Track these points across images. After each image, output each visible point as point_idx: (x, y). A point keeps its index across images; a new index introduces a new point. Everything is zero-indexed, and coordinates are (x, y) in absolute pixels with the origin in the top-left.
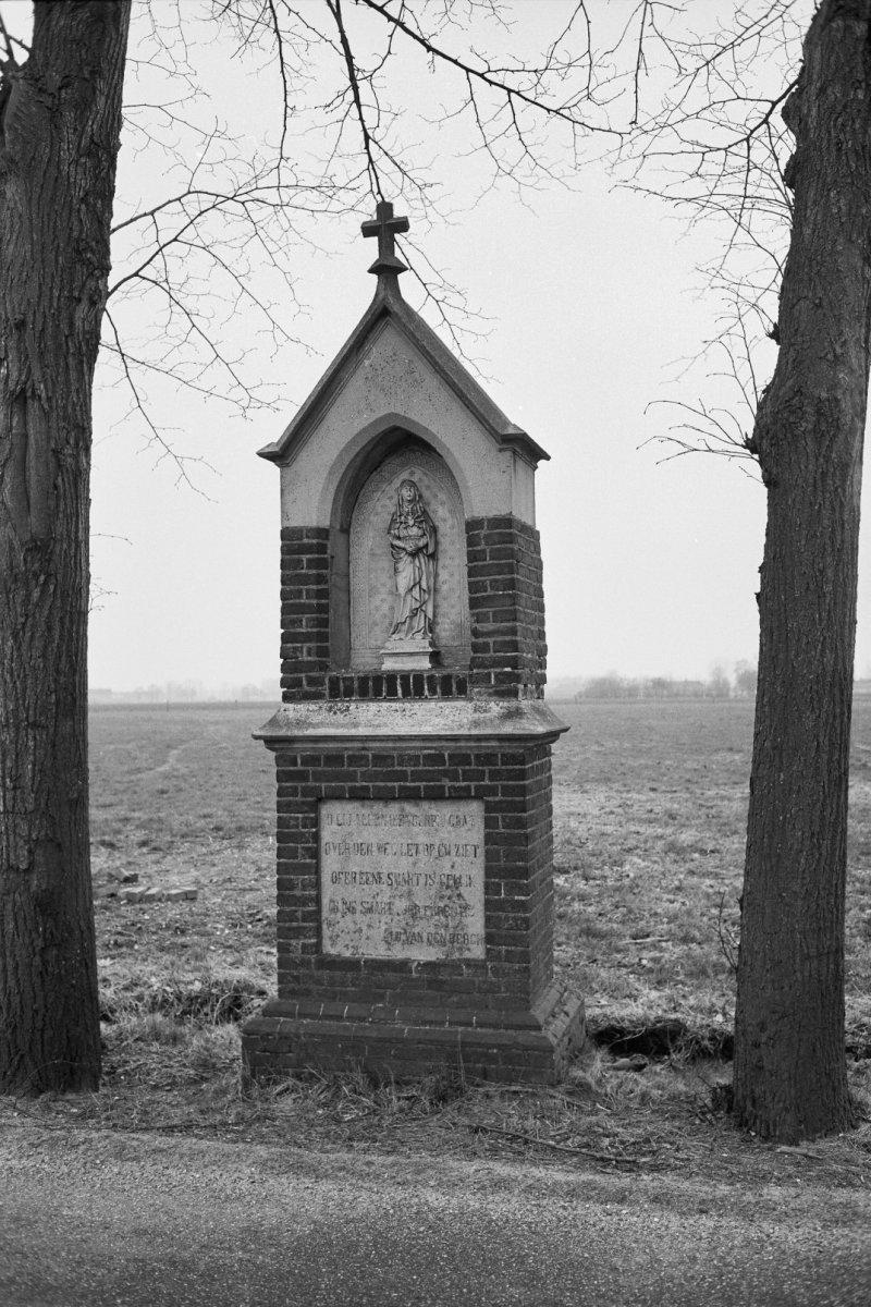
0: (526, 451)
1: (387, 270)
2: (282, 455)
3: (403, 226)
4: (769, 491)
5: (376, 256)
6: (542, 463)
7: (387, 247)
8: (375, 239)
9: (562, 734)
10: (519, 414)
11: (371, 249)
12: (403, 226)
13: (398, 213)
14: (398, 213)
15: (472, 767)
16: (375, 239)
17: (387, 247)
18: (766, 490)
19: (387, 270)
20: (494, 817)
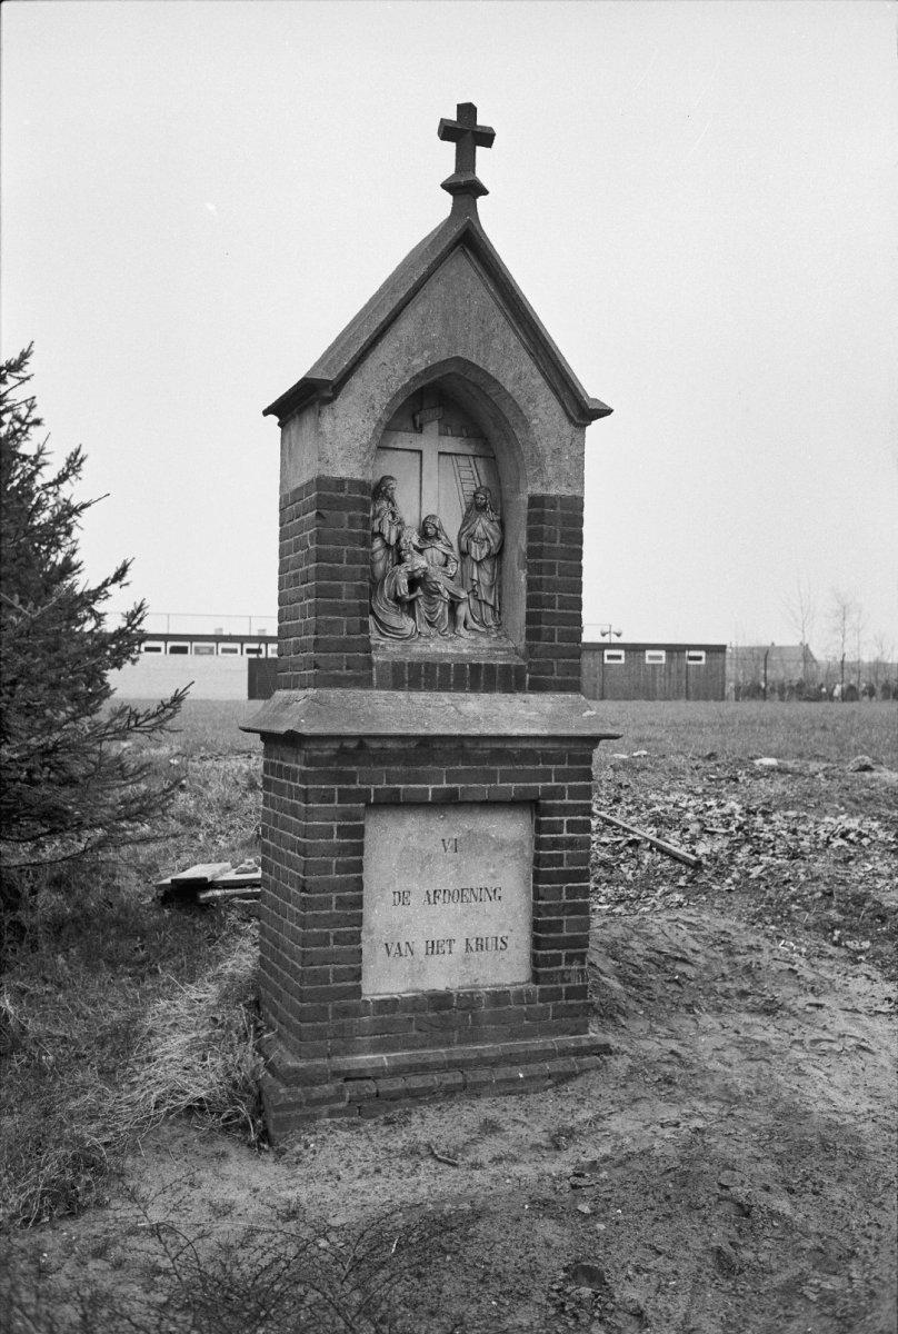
0: (584, 412)
1: (465, 189)
2: (297, 405)
3: (487, 138)
4: (454, 200)
5: (452, 171)
6: (595, 430)
7: (465, 161)
8: (452, 146)
9: (603, 742)
10: (593, 387)
11: (445, 157)
12: (487, 138)
13: (482, 120)
14: (482, 120)
15: (566, 819)
16: (452, 146)
17: (465, 161)
18: (451, 197)
19: (465, 189)
20: (572, 864)
